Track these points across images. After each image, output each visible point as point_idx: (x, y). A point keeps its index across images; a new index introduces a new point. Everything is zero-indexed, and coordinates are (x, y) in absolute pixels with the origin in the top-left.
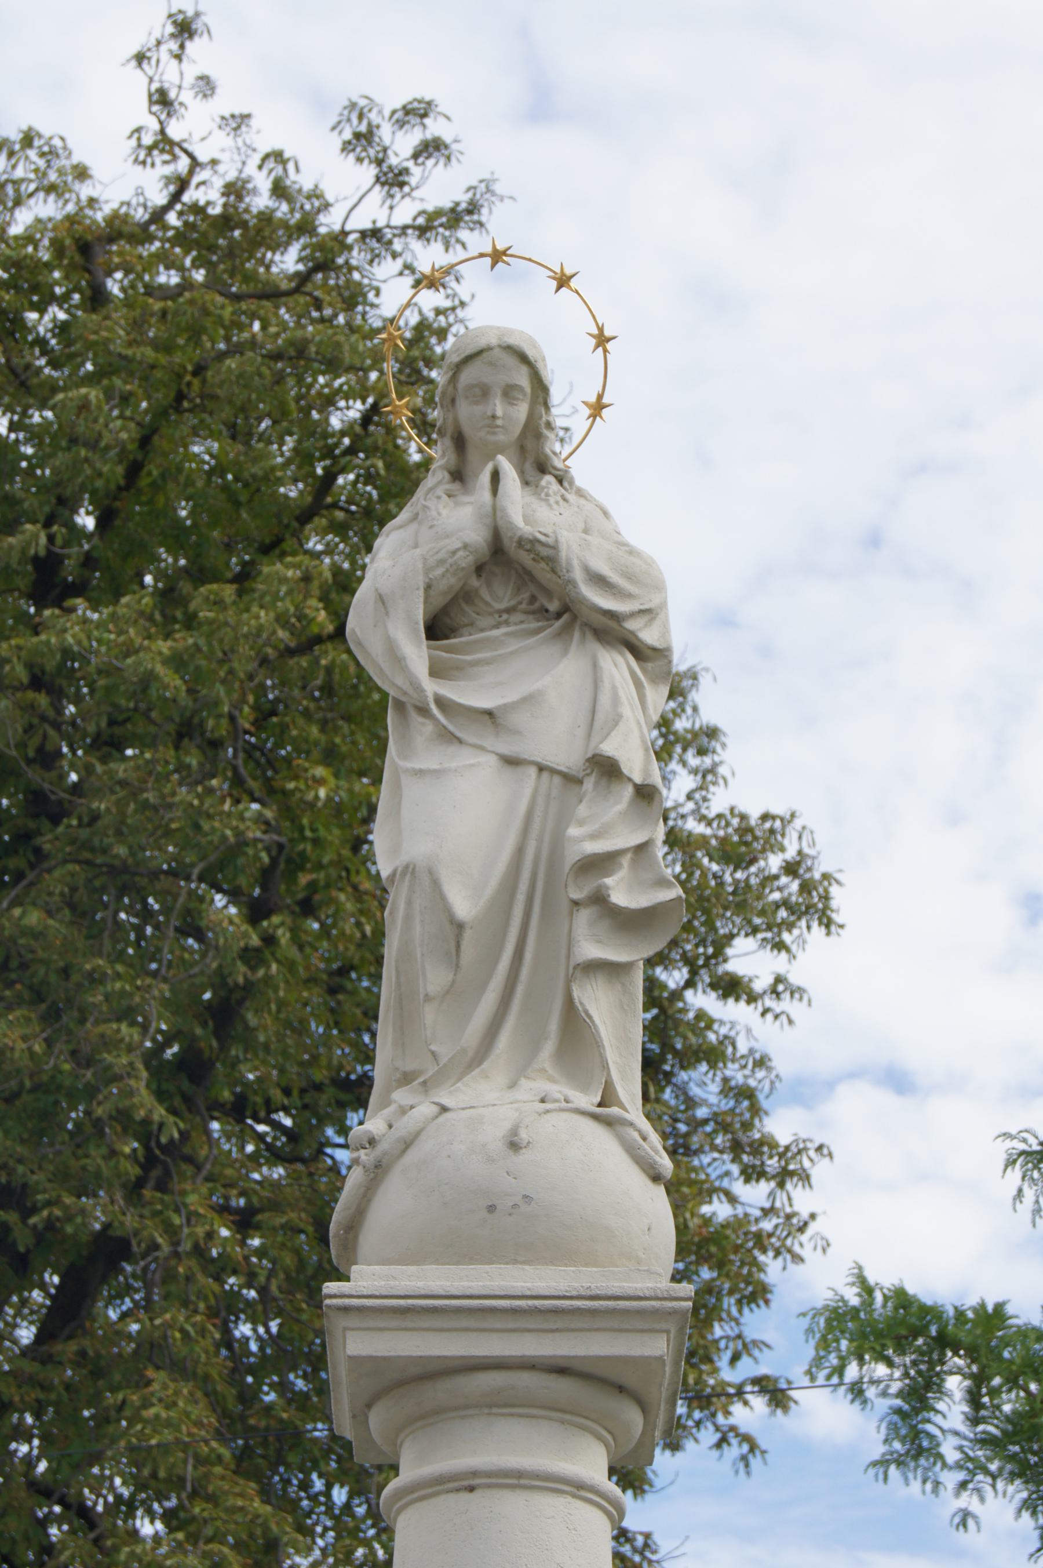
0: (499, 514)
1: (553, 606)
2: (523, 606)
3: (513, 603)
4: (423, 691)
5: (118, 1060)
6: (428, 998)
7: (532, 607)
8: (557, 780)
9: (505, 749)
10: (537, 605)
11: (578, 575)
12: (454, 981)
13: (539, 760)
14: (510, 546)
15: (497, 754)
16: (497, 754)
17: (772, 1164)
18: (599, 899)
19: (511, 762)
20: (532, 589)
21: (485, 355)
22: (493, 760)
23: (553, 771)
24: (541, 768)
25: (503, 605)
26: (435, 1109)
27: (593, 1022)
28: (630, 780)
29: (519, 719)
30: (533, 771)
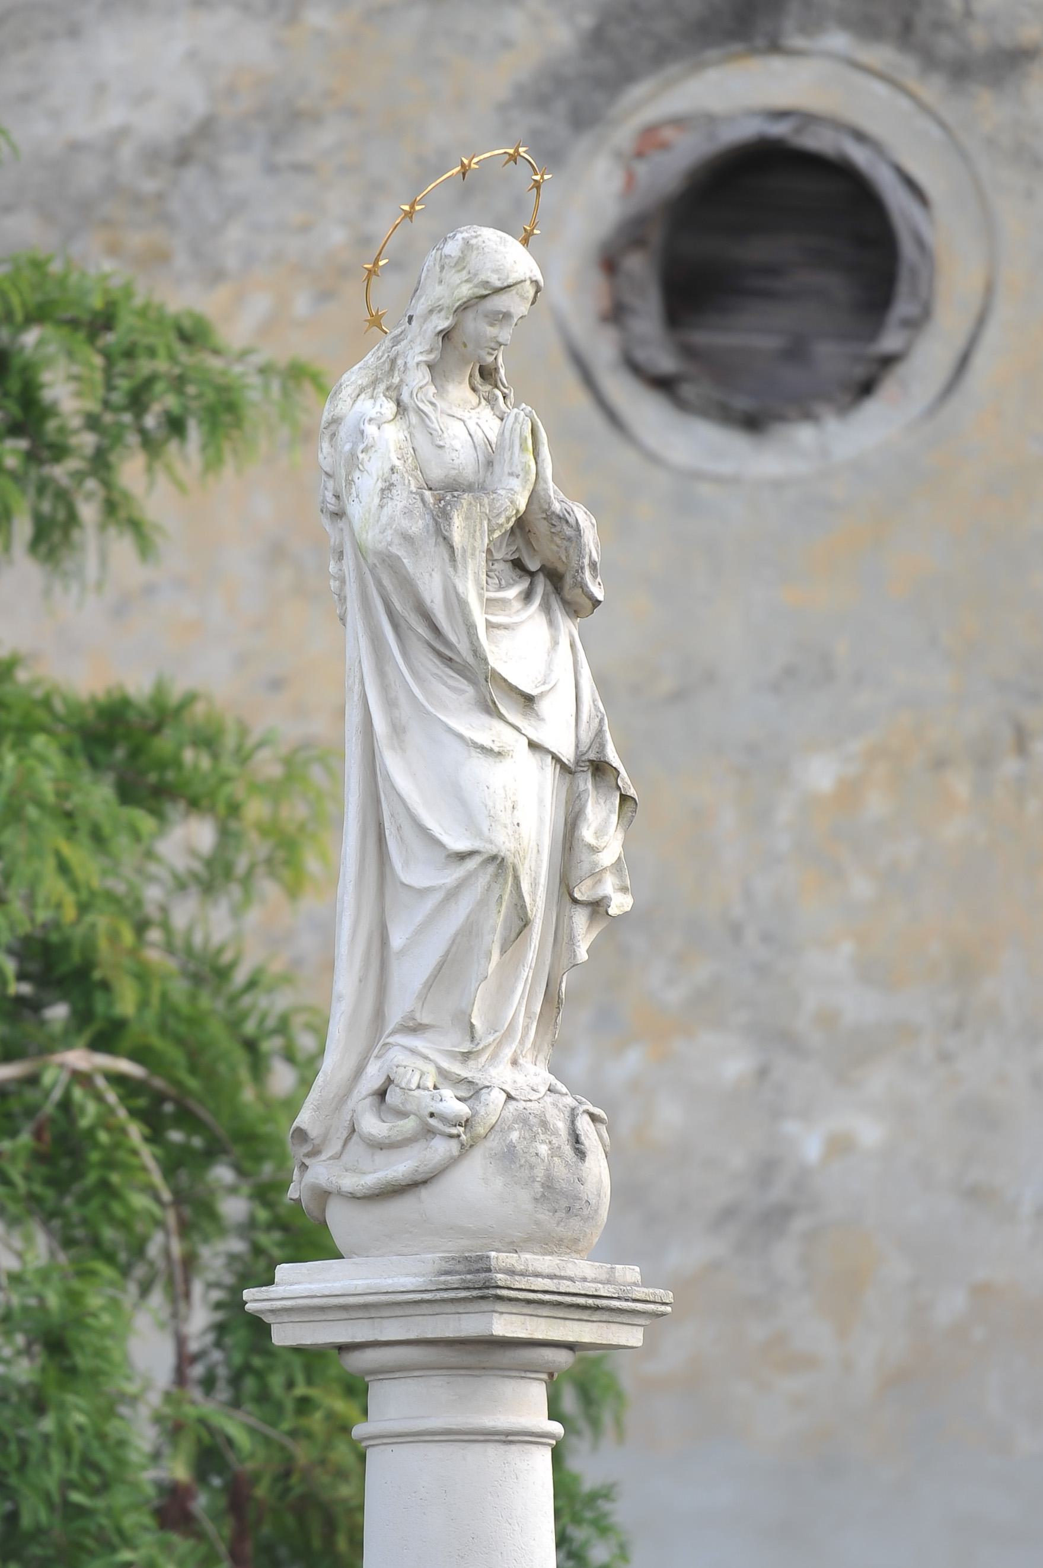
0: (539, 488)
9: (535, 737)
17: (564, 1203)
26: (504, 1096)
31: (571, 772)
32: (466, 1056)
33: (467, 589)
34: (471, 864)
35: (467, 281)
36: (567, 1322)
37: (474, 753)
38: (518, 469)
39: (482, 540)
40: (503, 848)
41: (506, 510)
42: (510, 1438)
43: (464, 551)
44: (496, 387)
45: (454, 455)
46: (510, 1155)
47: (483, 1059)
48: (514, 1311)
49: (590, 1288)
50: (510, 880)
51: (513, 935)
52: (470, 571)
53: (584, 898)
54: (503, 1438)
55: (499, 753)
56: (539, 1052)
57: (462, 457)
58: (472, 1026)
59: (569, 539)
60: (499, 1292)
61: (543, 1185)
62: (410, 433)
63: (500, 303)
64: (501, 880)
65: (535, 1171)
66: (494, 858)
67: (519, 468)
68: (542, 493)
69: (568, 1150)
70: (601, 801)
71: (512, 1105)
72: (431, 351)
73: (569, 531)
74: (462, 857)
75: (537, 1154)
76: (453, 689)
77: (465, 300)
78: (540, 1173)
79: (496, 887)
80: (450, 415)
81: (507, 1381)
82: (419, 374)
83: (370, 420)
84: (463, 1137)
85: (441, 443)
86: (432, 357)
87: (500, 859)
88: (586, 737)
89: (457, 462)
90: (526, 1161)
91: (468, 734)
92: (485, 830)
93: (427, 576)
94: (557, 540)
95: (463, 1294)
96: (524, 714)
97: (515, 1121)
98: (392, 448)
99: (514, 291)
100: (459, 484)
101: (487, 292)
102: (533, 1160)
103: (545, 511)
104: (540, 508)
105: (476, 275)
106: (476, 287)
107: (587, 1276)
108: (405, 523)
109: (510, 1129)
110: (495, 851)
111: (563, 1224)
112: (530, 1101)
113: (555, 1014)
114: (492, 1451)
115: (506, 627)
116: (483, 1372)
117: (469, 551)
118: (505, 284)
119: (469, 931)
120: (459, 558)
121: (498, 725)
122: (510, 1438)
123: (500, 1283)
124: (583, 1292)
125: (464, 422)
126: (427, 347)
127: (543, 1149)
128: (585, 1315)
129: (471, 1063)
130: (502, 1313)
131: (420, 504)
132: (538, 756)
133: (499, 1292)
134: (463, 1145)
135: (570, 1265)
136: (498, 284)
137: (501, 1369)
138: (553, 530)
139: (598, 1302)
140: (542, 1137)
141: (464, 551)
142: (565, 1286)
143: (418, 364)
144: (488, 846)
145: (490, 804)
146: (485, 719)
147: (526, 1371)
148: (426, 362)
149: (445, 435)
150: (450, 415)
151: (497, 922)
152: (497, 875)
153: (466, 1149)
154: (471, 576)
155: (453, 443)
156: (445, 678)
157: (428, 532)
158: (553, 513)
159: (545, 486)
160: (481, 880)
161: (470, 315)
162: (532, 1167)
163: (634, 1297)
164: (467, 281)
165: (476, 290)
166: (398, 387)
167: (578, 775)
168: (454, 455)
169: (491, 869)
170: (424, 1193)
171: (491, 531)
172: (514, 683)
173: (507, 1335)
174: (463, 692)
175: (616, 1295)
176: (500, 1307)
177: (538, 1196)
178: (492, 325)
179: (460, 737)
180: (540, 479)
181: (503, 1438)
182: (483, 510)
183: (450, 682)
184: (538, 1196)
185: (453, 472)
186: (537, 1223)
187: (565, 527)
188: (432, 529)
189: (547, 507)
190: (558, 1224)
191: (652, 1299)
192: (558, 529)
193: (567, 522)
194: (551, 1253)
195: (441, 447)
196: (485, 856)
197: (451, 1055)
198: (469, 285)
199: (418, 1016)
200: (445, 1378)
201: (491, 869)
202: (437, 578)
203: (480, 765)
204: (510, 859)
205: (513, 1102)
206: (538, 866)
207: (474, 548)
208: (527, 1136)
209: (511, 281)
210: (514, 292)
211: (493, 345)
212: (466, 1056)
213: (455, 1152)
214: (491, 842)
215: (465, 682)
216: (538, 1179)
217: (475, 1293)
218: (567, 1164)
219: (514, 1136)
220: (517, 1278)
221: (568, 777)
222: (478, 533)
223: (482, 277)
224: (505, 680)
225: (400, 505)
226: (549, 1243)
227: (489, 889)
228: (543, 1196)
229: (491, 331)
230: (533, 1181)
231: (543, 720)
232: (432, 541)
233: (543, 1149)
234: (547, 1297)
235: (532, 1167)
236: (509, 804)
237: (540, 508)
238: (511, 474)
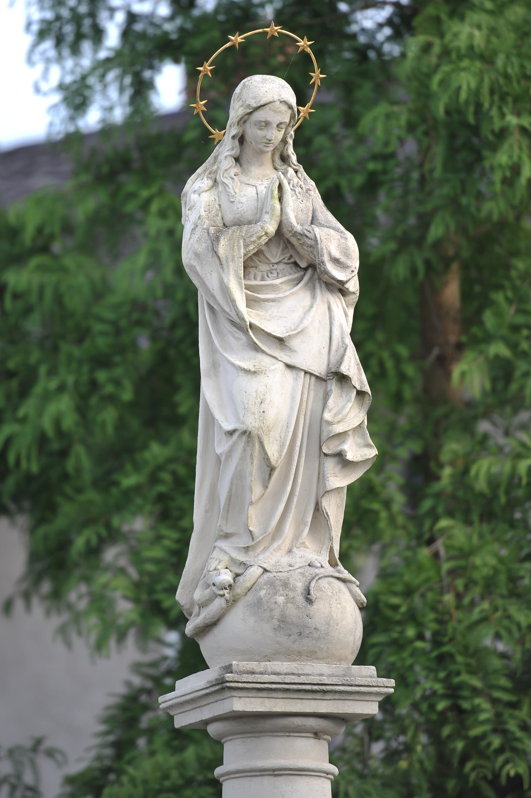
0: (284, 218)
1: (303, 265)
2: (286, 261)
3: (281, 258)
4: (245, 321)
5: (408, 702)
6: (251, 503)
7: (290, 261)
8: (313, 379)
9: (289, 362)
10: (292, 260)
11: (326, 258)
12: (264, 494)
13: (306, 369)
14: (285, 230)
15: (284, 363)
16: (284, 363)
17: (295, 630)
18: (340, 456)
19: (289, 367)
20: (292, 252)
21: (270, 105)
22: (281, 366)
23: (311, 374)
24: (306, 372)
25: (276, 261)
26: (261, 570)
27: (329, 518)
28: (355, 387)
29: (295, 343)
30: (303, 373)
31: (325, 381)
32: (247, 549)
33: (229, 279)
34: (235, 436)
35: (241, 106)
36: (304, 701)
37: (241, 374)
38: (268, 210)
39: (239, 251)
40: (250, 426)
41: (257, 232)
42: (276, 773)
43: (227, 258)
44: (290, 166)
45: (239, 205)
46: (259, 603)
47: (259, 550)
48: (250, 695)
49: (316, 680)
50: (257, 445)
51: (267, 476)
52: (231, 270)
53: (330, 452)
54: (271, 773)
55: (255, 372)
56: (323, 545)
57: (245, 206)
58: (250, 531)
59: (311, 246)
60: (228, 684)
61: (279, 621)
62: (218, 196)
63: (259, 116)
64: (250, 444)
65: (274, 612)
66: (245, 432)
67: (269, 208)
68: (285, 221)
69: (300, 599)
70: (344, 396)
71: (266, 576)
72: (233, 149)
73: (310, 242)
74: (231, 433)
75: (276, 603)
76: (237, 339)
77: (240, 117)
78: (277, 614)
79: (249, 449)
80: (246, 184)
81: (277, 739)
82: (227, 163)
83: (195, 191)
84: (227, 595)
85: (232, 200)
86: (234, 152)
87: (248, 433)
88: (333, 360)
89: (240, 209)
90: (268, 607)
91: (237, 363)
92: (241, 416)
93: (209, 275)
94: (304, 247)
95: (213, 689)
96: (282, 349)
97: (265, 584)
98: (203, 206)
99: (267, 108)
100: (241, 222)
101: (251, 110)
102: (273, 606)
103: (291, 232)
104: (288, 230)
105: (245, 102)
106: (245, 108)
107: (324, 673)
108: (196, 246)
109: (261, 589)
110: (245, 428)
111: (297, 643)
112: (281, 572)
113: (326, 522)
114: (267, 781)
115: (273, 300)
116: (260, 734)
117: (230, 258)
118: (259, 105)
119: (239, 476)
120: (224, 263)
121: (260, 356)
122: (276, 773)
123: (227, 679)
124: (308, 682)
125: (256, 187)
126: (231, 147)
127: (281, 599)
128: (310, 696)
129: (251, 553)
130: (240, 697)
131: (206, 235)
132: (294, 372)
133: (228, 684)
134: (227, 600)
135: (308, 667)
136: (255, 105)
137: (271, 732)
138: (300, 242)
139: (324, 688)
140: (281, 592)
141: (227, 258)
142: (303, 679)
143: (226, 157)
144: (242, 426)
145: (246, 401)
146: (253, 354)
147: (289, 732)
148: (231, 156)
149: (238, 194)
150: (246, 184)
151: (254, 469)
152: (248, 442)
153: (233, 602)
154: (232, 272)
155: (241, 199)
156: (234, 333)
157: (208, 250)
158: (296, 232)
159: (286, 217)
160: (240, 446)
161: (248, 125)
162: (271, 610)
163: (357, 683)
164: (241, 106)
165: (245, 110)
166: (216, 172)
167: (328, 382)
168: (239, 205)
169: (244, 438)
170: (216, 631)
171: (246, 246)
172: (269, 331)
173: (246, 710)
174: (241, 339)
175: (341, 683)
176: (234, 693)
177: (276, 627)
178: (261, 129)
179: (233, 365)
180: (284, 214)
181: (271, 773)
182: (241, 234)
183: (236, 335)
184: (276, 627)
185: (238, 215)
186: (278, 643)
187: (306, 240)
188: (210, 248)
189: (290, 229)
190: (294, 643)
191: (374, 684)
192: (302, 241)
193: (307, 237)
194: (295, 660)
195: (232, 202)
196: (240, 432)
197: (239, 549)
198: (242, 108)
199: (224, 528)
200: (242, 740)
201: (244, 438)
202: (215, 276)
203: (243, 381)
204: (255, 432)
205: (268, 574)
206: (286, 435)
207: (233, 256)
208: (271, 592)
209: (262, 103)
210: (267, 109)
211: (265, 141)
212: (247, 549)
213: (224, 604)
214: (243, 423)
215: (241, 334)
216: (276, 617)
217: (217, 688)
218: (298, 607)
219: (263, 593)
220: (244, 675)
221: (324, 383)
222: (236, 247)
223: (247, 103)
224: (263, 330)
225: (197, 236)
226: (289, 655)
227: (244, 450)
228: (280, 627)
229: (261, 133)
230: (272, 619)
231: (295, 351)
232: (210, 255)
233: (281, 599)
234: (274, 686)
235: (271, 610)
236: (259, 400)
237: (288, 230)
238: (266, 213)
